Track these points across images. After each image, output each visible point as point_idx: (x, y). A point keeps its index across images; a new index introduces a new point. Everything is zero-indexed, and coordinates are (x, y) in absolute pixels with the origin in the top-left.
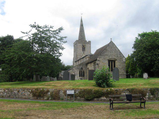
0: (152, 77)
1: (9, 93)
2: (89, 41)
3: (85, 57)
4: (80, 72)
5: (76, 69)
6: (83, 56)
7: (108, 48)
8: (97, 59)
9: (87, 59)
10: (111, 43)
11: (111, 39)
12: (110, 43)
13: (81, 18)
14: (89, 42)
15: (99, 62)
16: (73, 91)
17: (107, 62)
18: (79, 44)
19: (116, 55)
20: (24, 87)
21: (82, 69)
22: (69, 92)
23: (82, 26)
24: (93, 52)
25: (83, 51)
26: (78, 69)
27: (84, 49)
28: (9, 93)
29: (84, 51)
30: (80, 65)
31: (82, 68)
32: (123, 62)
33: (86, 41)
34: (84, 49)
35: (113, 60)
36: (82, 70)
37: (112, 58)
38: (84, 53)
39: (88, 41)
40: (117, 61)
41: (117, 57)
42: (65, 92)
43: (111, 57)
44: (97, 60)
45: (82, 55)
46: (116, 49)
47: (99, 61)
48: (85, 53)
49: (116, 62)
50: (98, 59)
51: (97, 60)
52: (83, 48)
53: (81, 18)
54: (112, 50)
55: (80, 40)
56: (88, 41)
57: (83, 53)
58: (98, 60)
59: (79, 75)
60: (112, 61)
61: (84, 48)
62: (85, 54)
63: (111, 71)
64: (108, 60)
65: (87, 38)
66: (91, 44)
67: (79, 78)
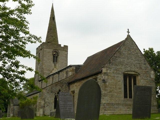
3: (65, 71)
6: (54, 72)
7: (123, 49)
8: (102, 71)
9: (70, 74)
10: (129, 38)
11: (128, 32)
12: (126, 39)
13: (53, 6)
14: (66, 47)
15: (106, 77)
17: (121, 78)
18: (48, 50)
20: (33, 93)
23: (53, 20)
24: (68, 66)
25: (54, 62)
27: (55, 58)
29: (56, 62)
30: (56, 84)
33: (60, 45)
34: (55, 58)
35: (132, 75)
37: (132, 70)
38: (55, 65)
39: (62, 46)
40: (139, 77)
41: (141, 68)
43: (129, 69)
44: (101, 72)
45: (51, 69)
46: (137, 53)
47: (107, 75)
48: (57, 65)
49: (138, 78)
50: (104, 70)
51: (101, 72)
53: (53, 6)
54: (130, 54)
55: (49, 42)
56: (62, 46)
58: (105, 73)
60: (130, 76)
61: (57, 57)
62: (57, 67)
64: (124, 74)
65: (62, 42)
66: (67, 51)
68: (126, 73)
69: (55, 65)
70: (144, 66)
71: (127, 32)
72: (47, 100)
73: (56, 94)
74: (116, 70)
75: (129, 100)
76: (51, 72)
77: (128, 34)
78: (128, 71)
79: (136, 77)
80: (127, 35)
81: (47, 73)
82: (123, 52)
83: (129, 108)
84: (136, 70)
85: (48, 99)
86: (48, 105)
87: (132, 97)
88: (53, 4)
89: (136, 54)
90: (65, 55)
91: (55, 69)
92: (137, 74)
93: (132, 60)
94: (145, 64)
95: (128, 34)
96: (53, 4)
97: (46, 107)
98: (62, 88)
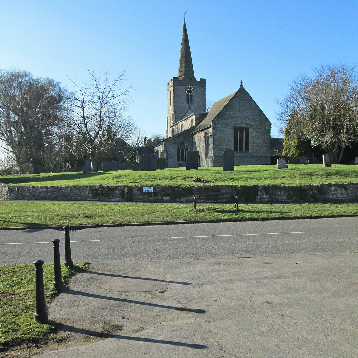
0: (339, 164)
1: (55, 192)
2: (201, 79)
4: (178, 151)
5: (170, 145)
16: (152, 188)
17: (232, 131)
19: (251, 117)
21: (183, 144)
22: (145, 190)
25: (188, 102)
26: (174, 144)
28: (55, 192)
29: (191, 101)
31: (183, 142)
32: (265, 130)
36: (182, 146)
38: (190, 108)
39: (198, 80)
42: (140, 189)
49: (251, 130)
52: (188, 95)
56: (198, 80)
57: (187, 105)
59: (176, 157)
60: (242, 129)
61: (191, 96)
63: (182, 161)
67: (177, 162)
68: (236, 126)
69: (190, 108)
70: (258, 117)
71: (243, 82)
72: (169, 153)
73: (179, 146)
74: (225, 124)
75: (240, 152)
76: (185, 116)
77: (241, 84)
78: (239, 124)
79: (248, 129)
80: (240, 86)
81: (179, 117)
82: (234, 105)
83: (238, 160)
84: (248, 122)
85: (170, 151)
86: (171, 157)
87: (238, 149)
88: (185, 19)
89: (249, 106)
90: (202, 93)
91: (190, 112)
92: (250, 126)
93: (244, 112)
94: (260, 115)
95: (241, 84)
96: (185, 19)
97: (169, 159)
98: (185, 139)
